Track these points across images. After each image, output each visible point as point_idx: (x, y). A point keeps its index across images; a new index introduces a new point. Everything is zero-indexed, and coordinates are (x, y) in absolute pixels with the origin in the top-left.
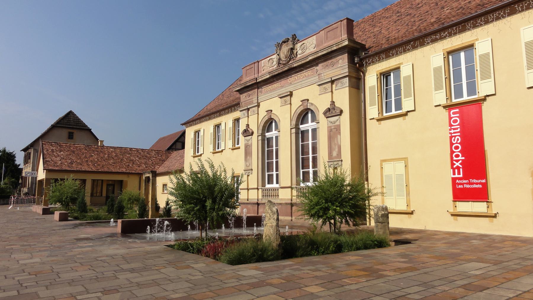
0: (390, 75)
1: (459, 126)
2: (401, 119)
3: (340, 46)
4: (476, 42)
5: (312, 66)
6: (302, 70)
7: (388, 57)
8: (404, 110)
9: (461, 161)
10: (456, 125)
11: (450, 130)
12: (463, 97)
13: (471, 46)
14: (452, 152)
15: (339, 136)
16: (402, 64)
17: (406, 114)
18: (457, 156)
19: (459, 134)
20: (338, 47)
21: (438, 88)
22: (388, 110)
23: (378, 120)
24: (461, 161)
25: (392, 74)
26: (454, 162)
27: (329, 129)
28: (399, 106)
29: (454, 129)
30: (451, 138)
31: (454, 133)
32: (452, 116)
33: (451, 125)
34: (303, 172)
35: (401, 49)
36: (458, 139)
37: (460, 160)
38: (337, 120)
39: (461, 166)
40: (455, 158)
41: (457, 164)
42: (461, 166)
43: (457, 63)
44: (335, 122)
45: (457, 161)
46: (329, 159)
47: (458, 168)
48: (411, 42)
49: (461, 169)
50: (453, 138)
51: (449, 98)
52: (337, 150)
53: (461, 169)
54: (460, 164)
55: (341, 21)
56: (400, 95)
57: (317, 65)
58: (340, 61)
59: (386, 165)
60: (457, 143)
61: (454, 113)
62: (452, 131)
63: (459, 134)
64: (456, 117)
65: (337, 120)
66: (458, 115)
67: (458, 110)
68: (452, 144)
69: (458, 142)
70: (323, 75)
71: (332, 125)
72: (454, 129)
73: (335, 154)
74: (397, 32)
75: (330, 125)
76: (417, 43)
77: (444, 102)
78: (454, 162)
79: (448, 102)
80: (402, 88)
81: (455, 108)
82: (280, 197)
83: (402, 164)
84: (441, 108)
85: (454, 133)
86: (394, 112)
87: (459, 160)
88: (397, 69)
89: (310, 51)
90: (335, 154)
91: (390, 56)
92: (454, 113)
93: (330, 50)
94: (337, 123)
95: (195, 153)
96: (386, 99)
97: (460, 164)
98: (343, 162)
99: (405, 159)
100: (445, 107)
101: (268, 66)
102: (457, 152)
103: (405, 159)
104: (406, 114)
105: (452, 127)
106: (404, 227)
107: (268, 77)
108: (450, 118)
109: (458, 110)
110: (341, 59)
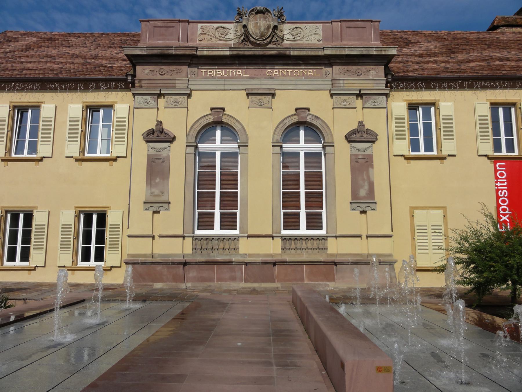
0: (28, 112)
1: (505, 180)
2: (33, 164)
3: (383, 53)
4: (116, 105)
5: (320, 65)
6: (299, 65)
7: (428, 87)
8: (114, 155)
9: (508, 216)
10: (503, 178)
11: (497, 182)
12: (96, 153)
13: (111, 106)
14: (498, 206)
15: (370, 169)
16: (116, 102)
17: (41, 160)
18: (504, 210)
19: (506, 188)
20: (379, 53)
21: (72, 139)
22: (19, 149)
23: (77, 160)
24: (508, 216)
25: (30, 111)
26: (501, 216)
27: (354, 157)
28: (33, 148)
29: (501, 182)
30: (497, 190)
31: (501, 186)
32: (498, 168)
33: (497, 178)
34: (199, 213)
35: (445, 84)
36: (505, 193)
37: (507, 214)
38: (368, 148)
39: (508, 220)
40: (501, 212)
41: (504, 218)
42: (508, 220)
43: (22, 120)
44: (365, 150)
45: (505, 215)
46: (352, 200)
47: (505, 221)
48: (13, 82)
49: (508, 224)
50: (500, 191)
51: (82, 152)
52: (366, 187)
53: (508, 224)
54: (507, 218)
55: (372, 21)
56: (37, 137)
57: (330, 65)
58: (372, 72)
59: (417, 214)
60: (504, 197)
61: (500, 166)
62: (499, 184)
63: (506, 188)
64: (502, 170)
65: (368, 148)
66: (504, 169)
67: (504, 164)
68: (498, 197)
69: (506, 196)
70: (341, 82)
71: (358, 153)
72: (501, 182)
73: (363, 193)
74: (435, 63)
75: (355, 152)
76: (466, 84)
77: (76, 155)
78: (501, 216)
79: (7, 156)
80: (40, 130)
81: (501, 162)
82: (242, 251)
83: (439, 214)
84: (485, 158)
85: (501, 186)
86: (25, 155)
87: (506, 214)
88: (109, 107)
89: (310, 42)
90: (363, 193)
91: (431, 88)
92: (500, 166)
93: (365, 52)
94: (368, 152)
95: (8, 151)
96: (18, 138)
97: (507, 218)
98: (171, 205)
99: (444, 208)
100: (490, 158)
101: (225, 36)
102: (504, 206)
103: (444, 208)
104: (41, 160)
105: (499, 180)
106: (434, 286)
107: (228, 53)
108: (496, 171)
109: (504, 164)
110: (374, 70)
